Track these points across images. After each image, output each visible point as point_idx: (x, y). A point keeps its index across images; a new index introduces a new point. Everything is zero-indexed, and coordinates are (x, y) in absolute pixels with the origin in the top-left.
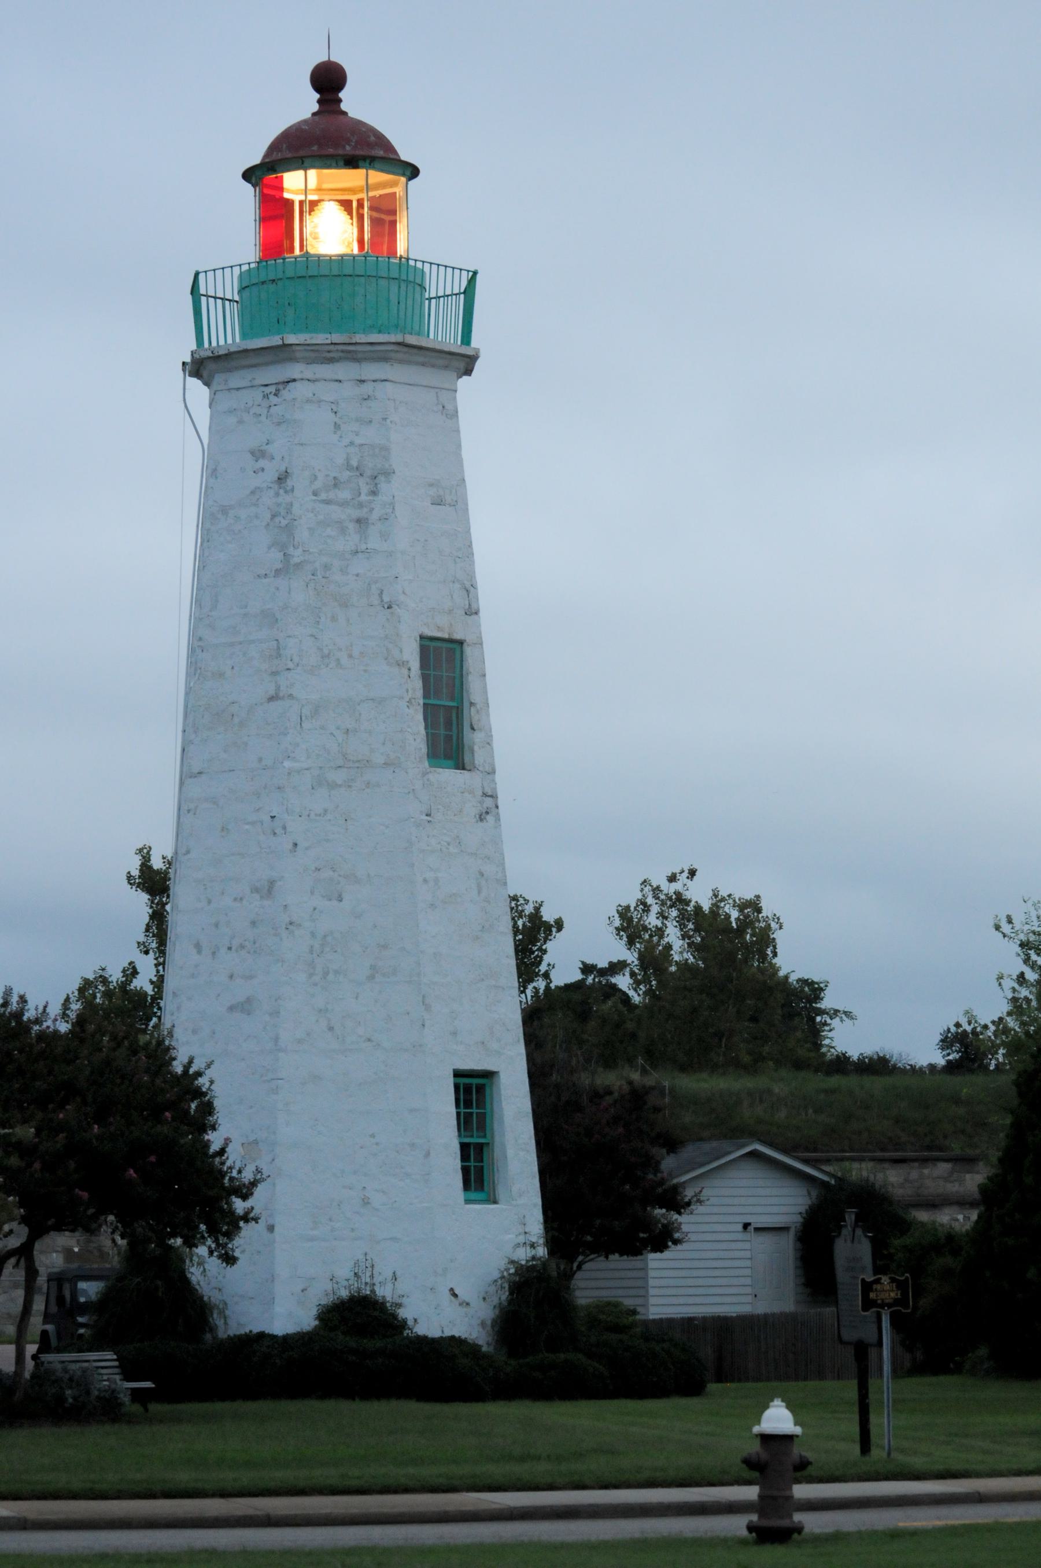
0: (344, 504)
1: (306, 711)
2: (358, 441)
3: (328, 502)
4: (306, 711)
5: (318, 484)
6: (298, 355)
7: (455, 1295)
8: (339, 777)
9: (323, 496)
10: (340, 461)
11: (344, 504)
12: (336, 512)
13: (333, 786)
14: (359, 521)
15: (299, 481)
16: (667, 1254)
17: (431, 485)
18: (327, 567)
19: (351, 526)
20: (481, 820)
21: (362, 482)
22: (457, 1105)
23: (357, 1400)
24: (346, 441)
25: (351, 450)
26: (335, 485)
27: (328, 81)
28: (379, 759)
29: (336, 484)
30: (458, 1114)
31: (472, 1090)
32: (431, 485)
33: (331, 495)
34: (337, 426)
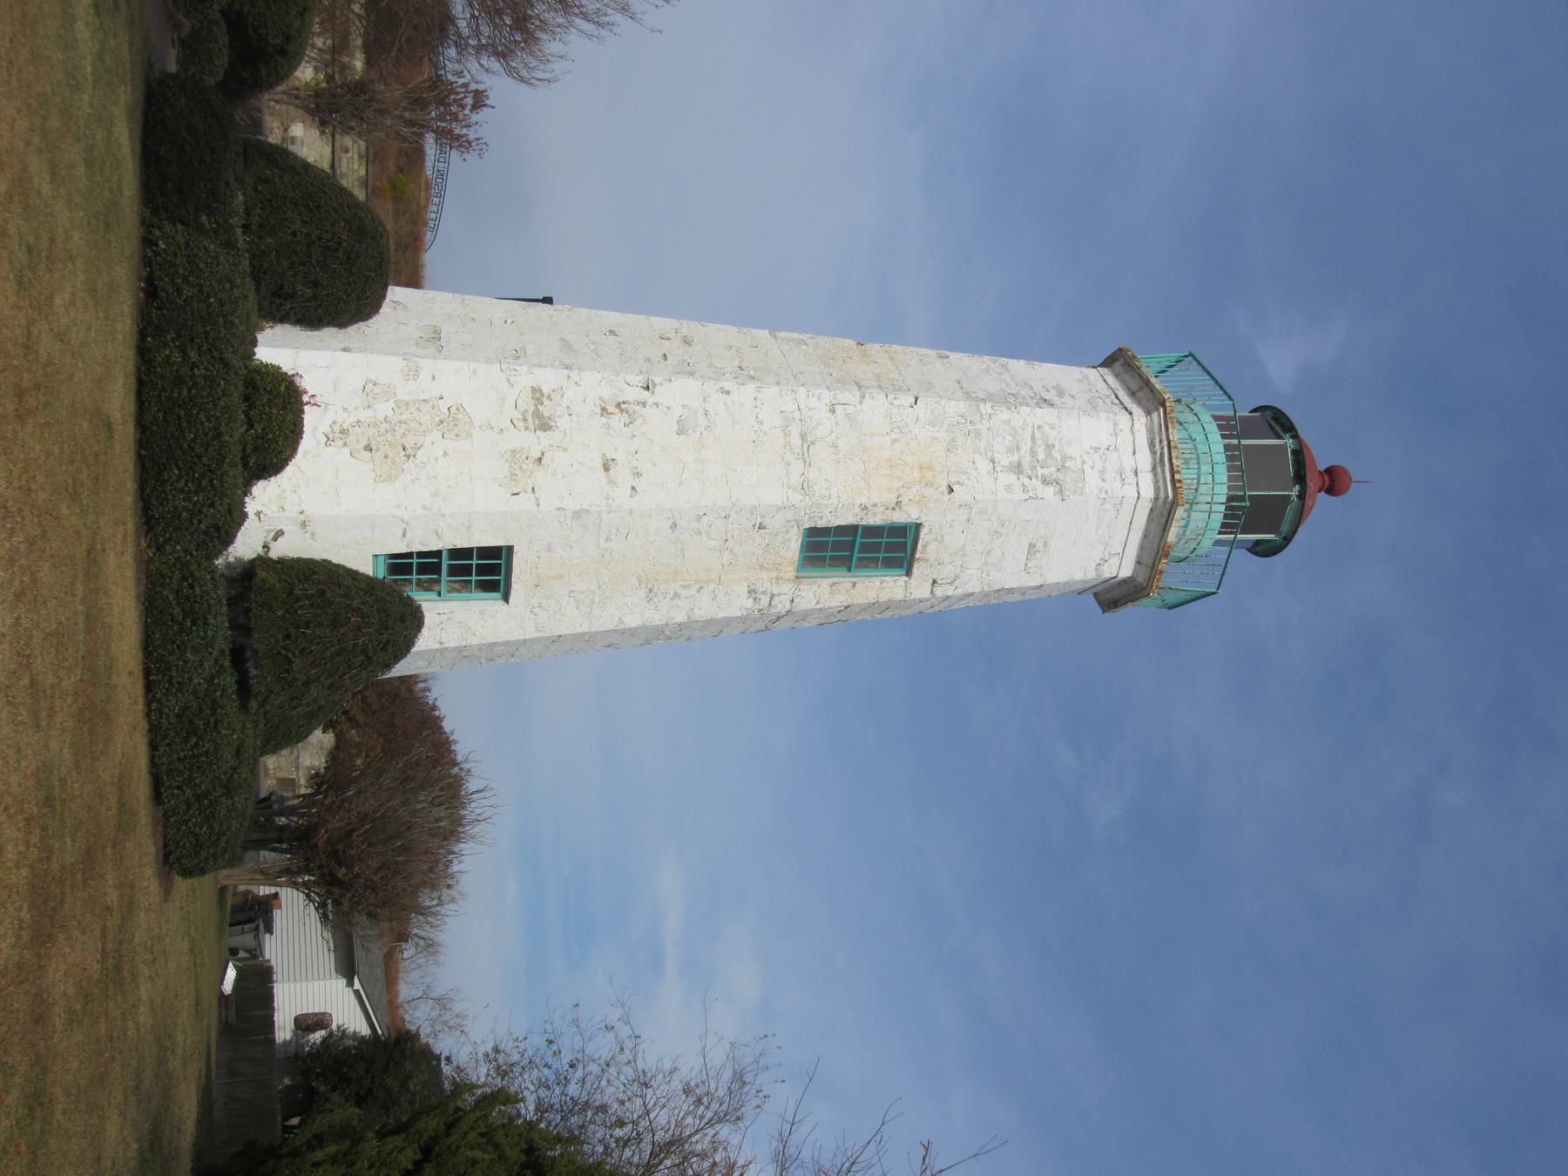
0: (1033, 453)
1: (851, 409)
2: (1087, 468)
3: (1033, 439)
4: (851, 409)
5: (1047, 429)
6: (1155, 415)
7: (275, 539)
8: (796, 440)
9: (1038, 435)
10: (1070, 451)
11: (1033, 453)
12: (1026, 445)
13: (784, 430)
14: (1019, 465)
15: (1044, 415)
16: (273, 963)
17: (1045, 544)
18: (978, 434)
19: (1015, 459)
20: (750, 592)
21: (1053, 469)
22: (421, 555)
23: (426, 900)
24: (1085, 457)
25: (1079, 461)
26: (1048, 446)
27: (1334, 481)
28: (812, 475)
29: (1049, 447)
30: (409, 555)
31: (891, 546)
32: (1045, 544)
33: (1039, 442)
34: (1097, 449)
